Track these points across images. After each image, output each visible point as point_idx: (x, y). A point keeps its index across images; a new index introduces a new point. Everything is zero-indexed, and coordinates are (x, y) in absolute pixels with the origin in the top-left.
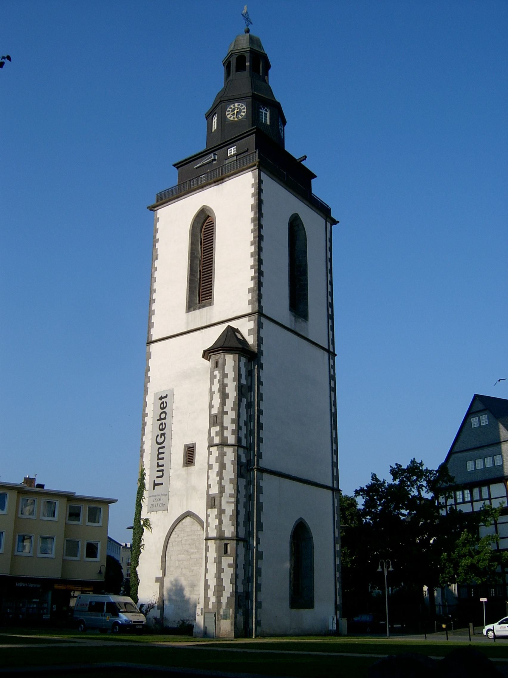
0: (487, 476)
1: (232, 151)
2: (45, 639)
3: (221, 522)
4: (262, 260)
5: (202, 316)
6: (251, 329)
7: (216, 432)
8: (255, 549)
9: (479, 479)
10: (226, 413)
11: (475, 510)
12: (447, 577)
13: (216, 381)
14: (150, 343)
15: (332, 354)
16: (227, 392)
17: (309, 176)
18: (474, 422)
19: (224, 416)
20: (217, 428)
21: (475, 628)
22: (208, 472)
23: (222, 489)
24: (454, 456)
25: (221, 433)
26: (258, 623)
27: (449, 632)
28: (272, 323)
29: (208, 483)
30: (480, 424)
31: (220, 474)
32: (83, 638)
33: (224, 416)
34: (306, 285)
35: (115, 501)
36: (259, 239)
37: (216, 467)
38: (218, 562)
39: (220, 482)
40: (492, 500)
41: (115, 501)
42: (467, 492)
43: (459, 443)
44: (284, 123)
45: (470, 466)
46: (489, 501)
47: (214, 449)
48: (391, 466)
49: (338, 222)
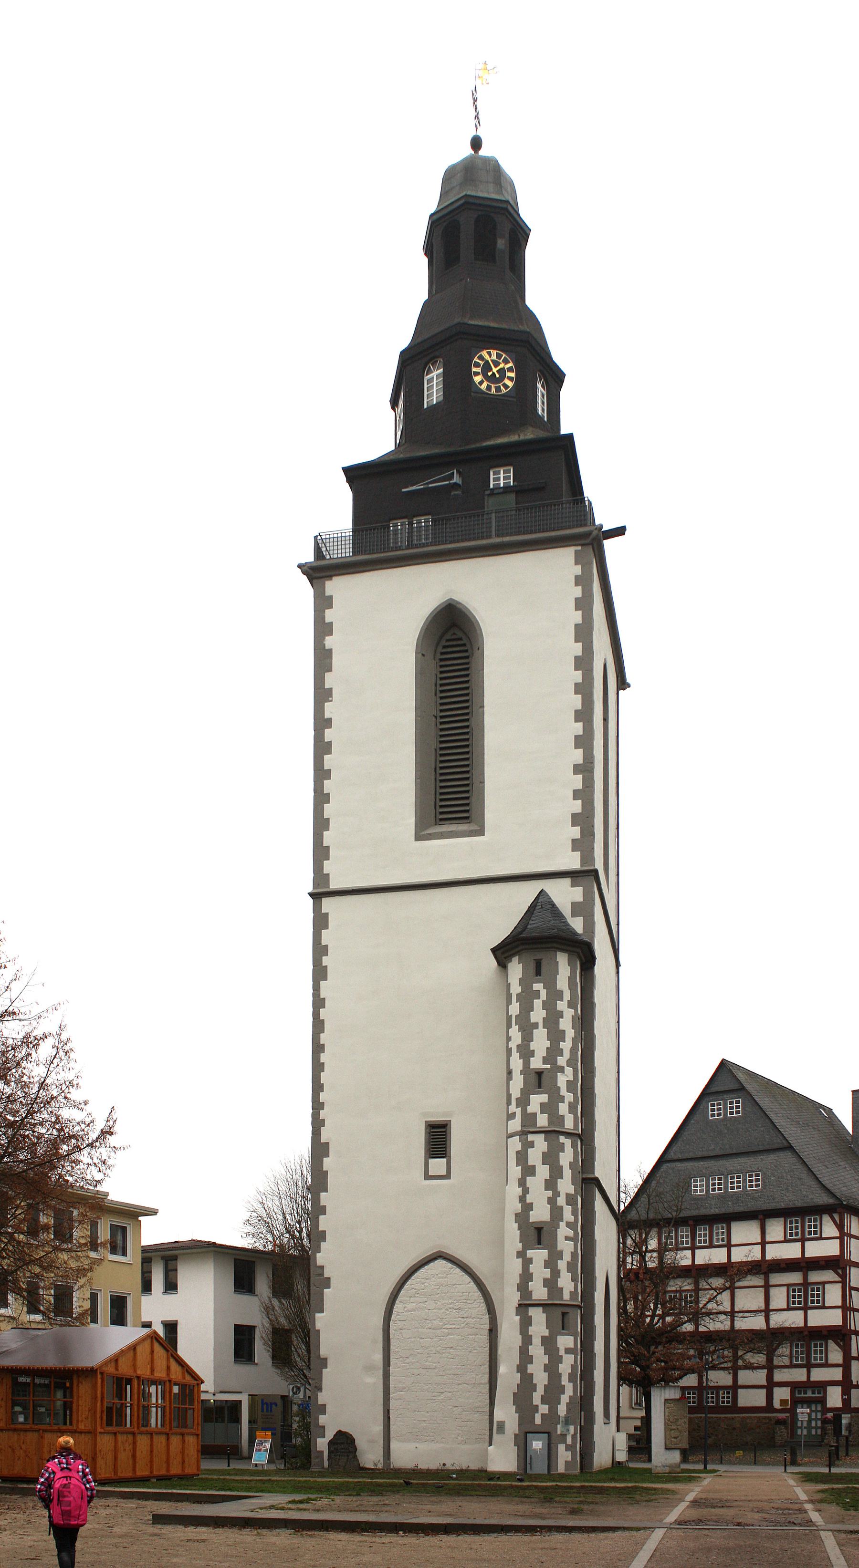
0: (731, 1207)
1: (501, 477)
2: (112, 1417)
3: (556, 1273)
4: (572, 1280)
5: (453, 854)
6: (578, 790)
7: (542, 1104)
8: (128, 1409)
9: (715, 1211)
10: (562, 1070)
11: (812, 1379)
12: (656, 1308)
13: (538, 1003)
14: (290, 1421)
15: (790, 1148)
16: (531, 1271)
17: (325, 978)
18: (714, 1111)
19: (529, 1150)
20: (544, 1098)
21: (431, 1161)
22: (618, 694)
23: (556, 1213)
24: (665, 1167)
25: (549, 1108)
26: (707, 1379)
27: (231, 1456)
28: (749, 1390)
29: (507, 1047)
30: (701, 1290)
31: (551, 1184)
32: (606, 720)
33: (529, 1150)
34: (531, 312)
35: (153, 1212)
36: (482, 556)
37: (543, 1172)
38: (549, 1343)
39: (552, 1201)
40: (733, 1249)
41: (153, 1212)
42: (406, 521)
43: (675, 1148)
44: (555, 378)
45: (698, 1188)
46: (690, 1252)
47: (709, 1467)
48: (620, 531)
49: (300, 566)
